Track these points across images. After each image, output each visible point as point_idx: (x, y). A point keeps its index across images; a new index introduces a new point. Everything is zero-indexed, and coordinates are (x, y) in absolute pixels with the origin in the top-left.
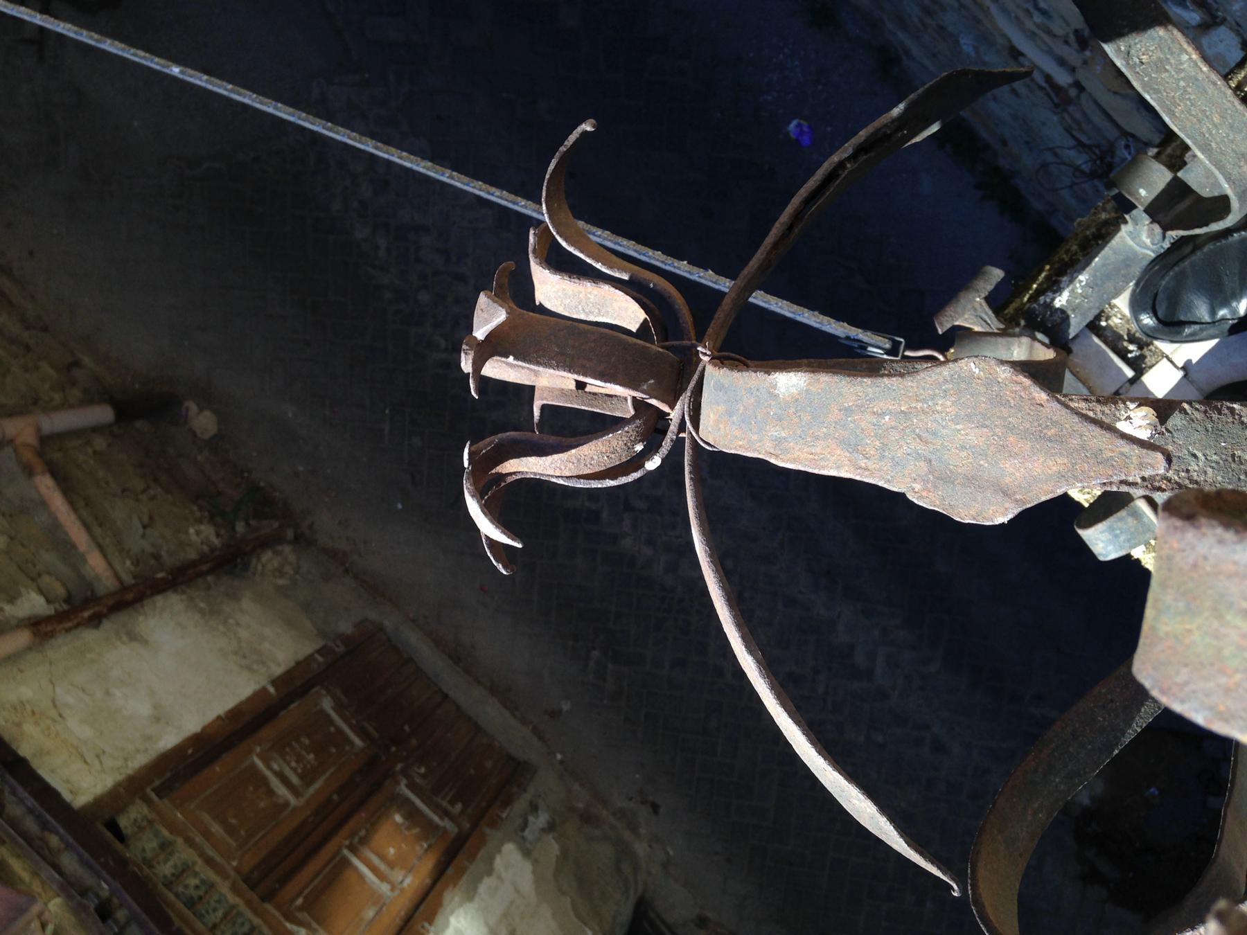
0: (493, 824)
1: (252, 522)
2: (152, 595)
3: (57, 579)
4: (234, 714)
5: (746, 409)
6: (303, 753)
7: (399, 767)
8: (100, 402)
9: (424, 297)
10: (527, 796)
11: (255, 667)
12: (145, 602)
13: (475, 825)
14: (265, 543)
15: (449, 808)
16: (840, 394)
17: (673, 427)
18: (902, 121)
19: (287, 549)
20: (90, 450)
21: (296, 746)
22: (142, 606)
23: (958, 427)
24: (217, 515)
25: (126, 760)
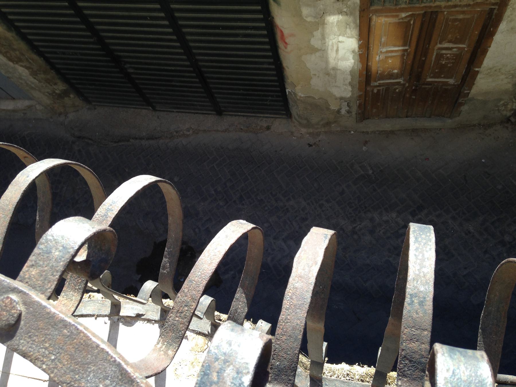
0: (360, 96)
10: (354, 113)
11: (489, 71)
13: (366, 92)
15: (379, 88)
19: (509, 114)
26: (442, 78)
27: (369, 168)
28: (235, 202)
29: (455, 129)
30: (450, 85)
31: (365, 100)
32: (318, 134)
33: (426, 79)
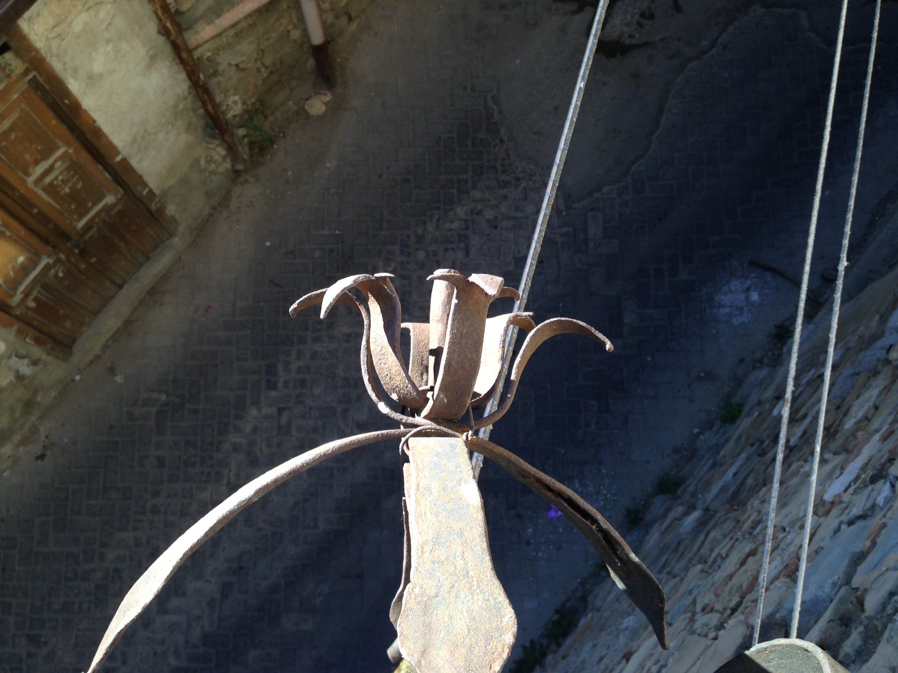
0: (20, 332)
1: (246, 140)
2: (187, 71)
3: (193, 5)
4: (98, 132)
5: (445, 465)
6: (70, 184)
7: (63, 256)
8: (325, 34)
9: (421, 255)
10: (44, 356)
11: (136, 146)
12: (181, 66)
13: (19, 319)
14: (231, 149)
15: (31, 297)
16: (471, 528)
17: (410, 420)
18: (626, 561)
19: (228, 165)
20: (290, 27)
21: (75, 179)
22: (177, 64)
23: (465, 613)
24: (250, 116)
25: (57, 56)
26: (92, 208)
27: (155, 395)
28: (29, 655)
29: (195, 241)
30: (113, 206)
31: (35, 328)
32: (34, 430)
33: (74, 228)
